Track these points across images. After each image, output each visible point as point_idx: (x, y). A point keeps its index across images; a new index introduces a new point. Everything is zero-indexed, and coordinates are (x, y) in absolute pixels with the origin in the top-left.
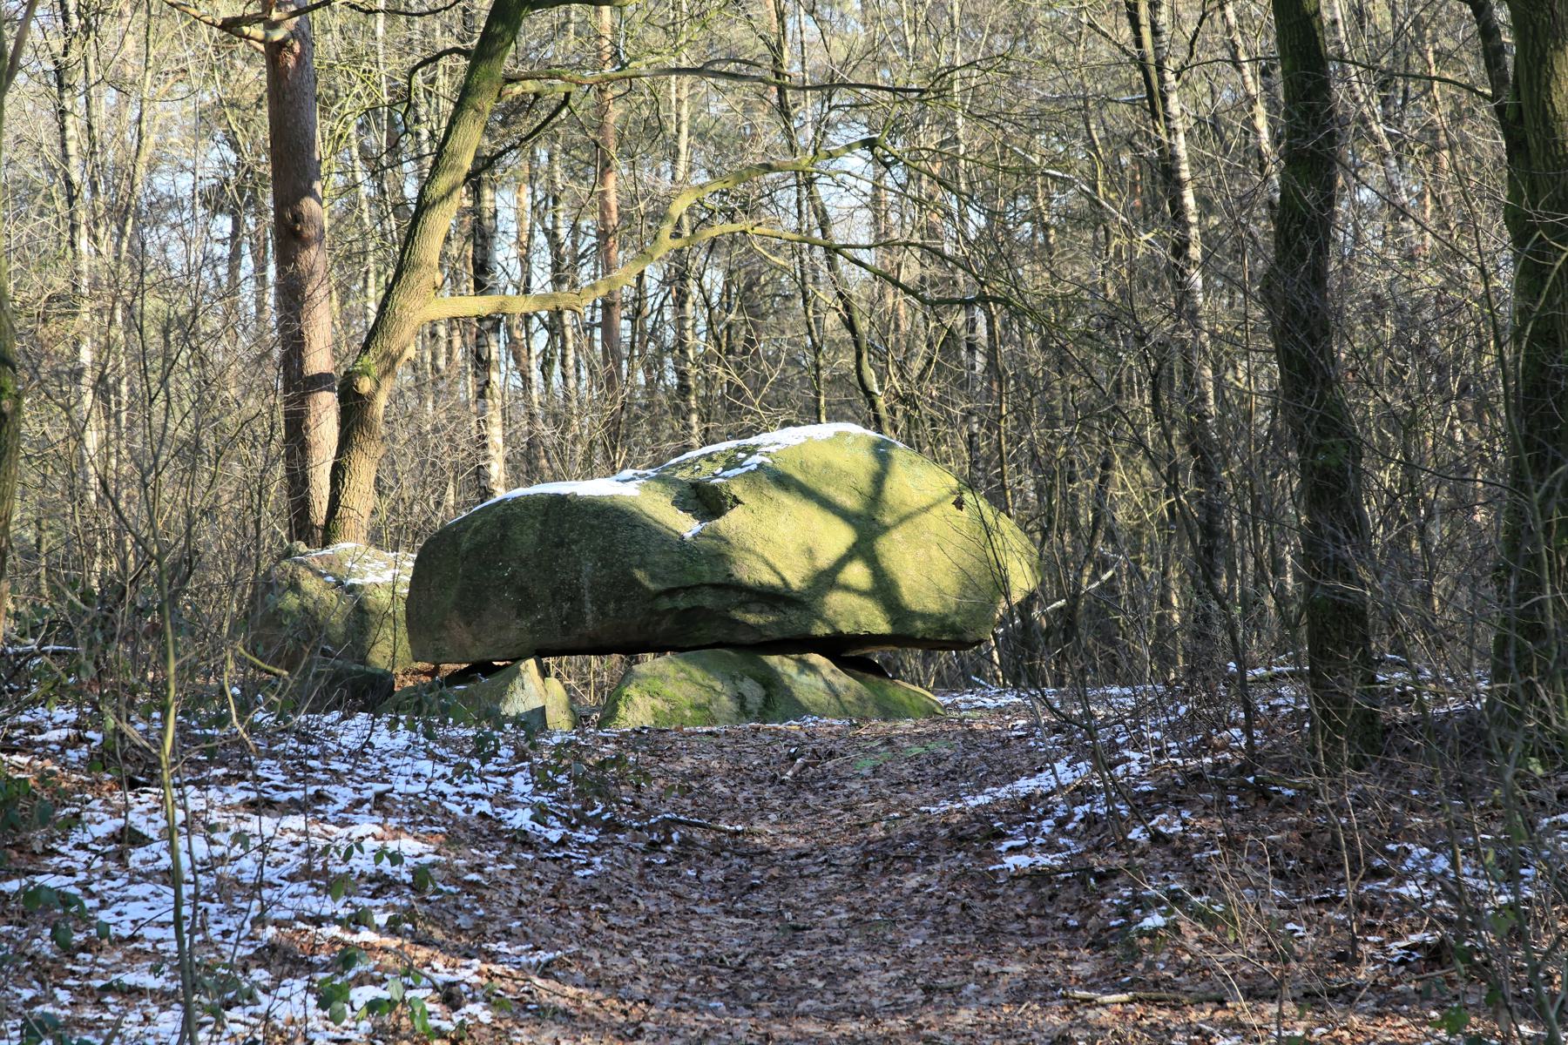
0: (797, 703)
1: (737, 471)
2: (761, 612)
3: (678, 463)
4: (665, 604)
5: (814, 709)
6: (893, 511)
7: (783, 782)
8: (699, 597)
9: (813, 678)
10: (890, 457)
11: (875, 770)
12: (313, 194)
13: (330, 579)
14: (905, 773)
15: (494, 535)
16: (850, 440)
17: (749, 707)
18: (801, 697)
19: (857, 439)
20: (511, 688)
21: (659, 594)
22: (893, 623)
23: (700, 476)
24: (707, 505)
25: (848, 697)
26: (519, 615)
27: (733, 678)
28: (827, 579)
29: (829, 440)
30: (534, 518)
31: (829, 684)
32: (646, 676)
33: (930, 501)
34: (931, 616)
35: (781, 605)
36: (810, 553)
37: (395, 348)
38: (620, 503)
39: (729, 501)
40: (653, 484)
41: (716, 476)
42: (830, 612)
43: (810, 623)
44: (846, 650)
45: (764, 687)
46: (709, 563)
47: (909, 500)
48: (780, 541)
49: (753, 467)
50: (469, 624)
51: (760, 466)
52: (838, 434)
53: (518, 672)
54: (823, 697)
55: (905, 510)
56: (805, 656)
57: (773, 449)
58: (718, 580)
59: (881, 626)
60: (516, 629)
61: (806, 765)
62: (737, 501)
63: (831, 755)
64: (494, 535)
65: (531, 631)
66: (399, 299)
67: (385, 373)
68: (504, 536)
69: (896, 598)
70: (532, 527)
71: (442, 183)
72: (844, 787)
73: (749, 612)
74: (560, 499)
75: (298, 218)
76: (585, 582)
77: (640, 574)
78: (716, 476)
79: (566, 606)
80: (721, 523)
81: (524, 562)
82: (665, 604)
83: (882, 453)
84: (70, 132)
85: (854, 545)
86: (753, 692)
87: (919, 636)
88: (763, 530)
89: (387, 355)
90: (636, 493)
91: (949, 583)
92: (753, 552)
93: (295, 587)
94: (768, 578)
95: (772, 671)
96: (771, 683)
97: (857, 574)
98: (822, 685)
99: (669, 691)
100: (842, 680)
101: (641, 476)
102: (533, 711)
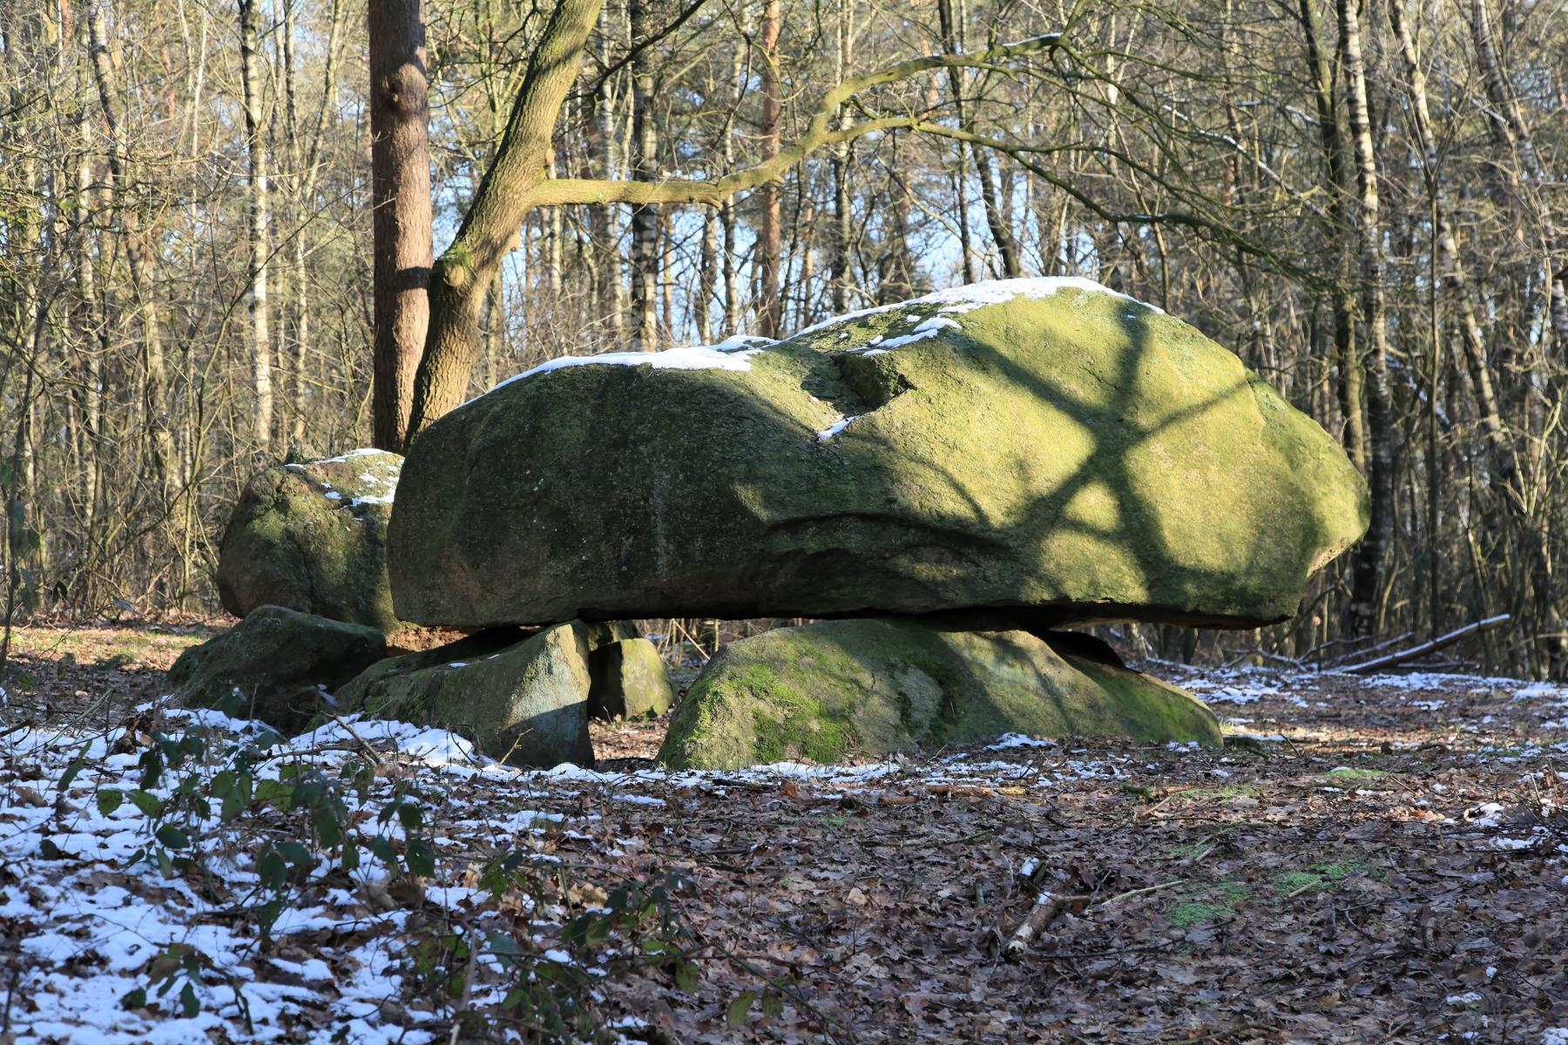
0: (995, 711)
1: (907, 339)
2: (939, 562)
3: (815, 332)
4: (785, 543)
5: (1021, 722)
6: (1151, 405)
7: (1010, 957)
8: (840, 535)
9: (1022, 673)
10: (1144, 327)
11: (1221, 931)
12: (415, 61)
13: (334, 495)
14: (1292, 942)
15: (520, 427)
16: (1081, 300)
17: (916, 716)
18: (999, 703)
19: (1092, 299)
20: (530, 671)
21: (774, 528)
22: (1151, 586)
23: (848, 347)
24: (856, 389)
25: (1075, 703)
26: (553, 554)
27: (890, 668)
28: (1048, 511)
29: (1049, 300)
30: (584, 401)
31: (1044, 681)
32: (748, 661)
33: (1208, 395)
34: (1209, 575)
35: (971, 552)
36: (1022, 467)
37: (496, 234)
38: (718, 380)
39: (892, 384)
40: (773, 355)
41: (872, 347)
42: (1051, 566)
43: (1019, 582)
44: (1074, 628)
45: (941, 683)
46: (859, 479)
47: (1175, 392)
48: (977, 449)
49: (932, 333)
50: (476, 566)
51: (944, 331)
52: (1062, 291)
53: (543, 647)
54: (1038, 704)
55: (1168, 408)
56: (1006, 635)
57: (963, 309)
58: (872, 507)
59: (1135, 592)
60: (548, 578)
61: (1058, 910)
62: (905, 384)
63: (1111, 882)
64: (520, 427)
65: (572, 579)
66: (503, 177)
67: (484, 264)
68: (535, 429)
69: (1154, 546)
70: (580, 415)
71: (560, 45)
72: (1155, 978)
73: (919, 560)
74: (627, 374)
75: (396, 87)
76: (658, 504)
77: (747, 495)
78: (872, 347)
79: (628, 542)
80: (879, 416)
81: (564, 471)
82: (785, 543)
83: (1132, 323)
84: (253, 73)
85: (1091, 460)
86: (924, 692)
87: (1190, 607)
88: (947, 431)
89: (487, 242)
90: (746, 367)
91: (1238, 525)
92: (930, 465)
93: (282, 506)
94: (951, 505)
95: (952, 655)
96: (952, 678)
97: (1095, 504)
98: (1033, 682)
99: (783, 687)
100: (1064, 674)
101: (756, 345)
102: (566, 709)
